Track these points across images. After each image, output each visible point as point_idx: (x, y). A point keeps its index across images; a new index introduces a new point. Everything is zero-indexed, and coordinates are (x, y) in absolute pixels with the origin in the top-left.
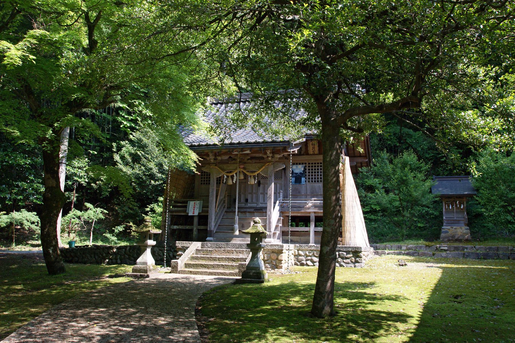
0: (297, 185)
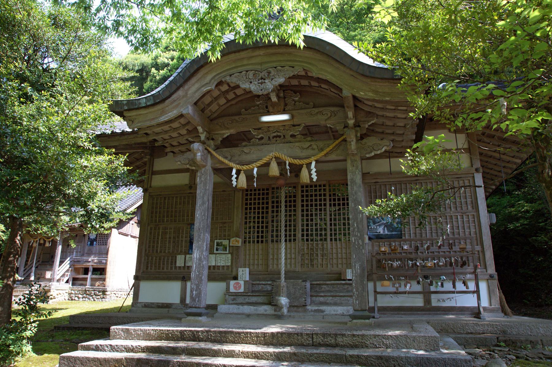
0: (91, 247)
